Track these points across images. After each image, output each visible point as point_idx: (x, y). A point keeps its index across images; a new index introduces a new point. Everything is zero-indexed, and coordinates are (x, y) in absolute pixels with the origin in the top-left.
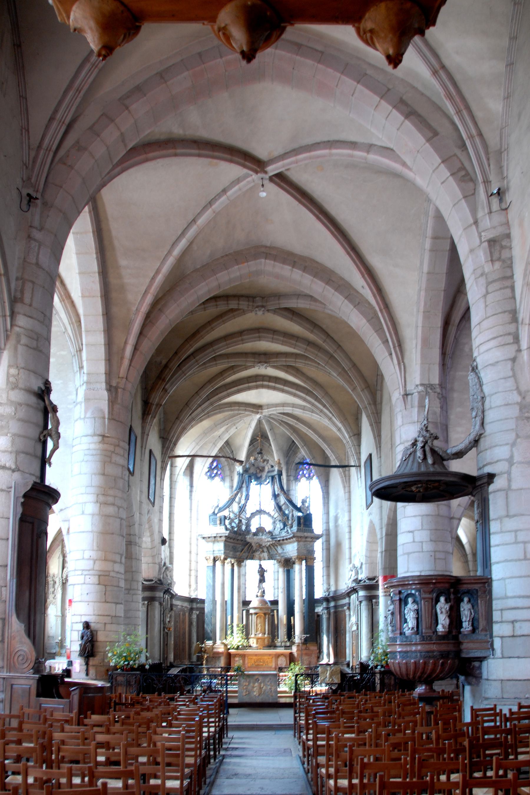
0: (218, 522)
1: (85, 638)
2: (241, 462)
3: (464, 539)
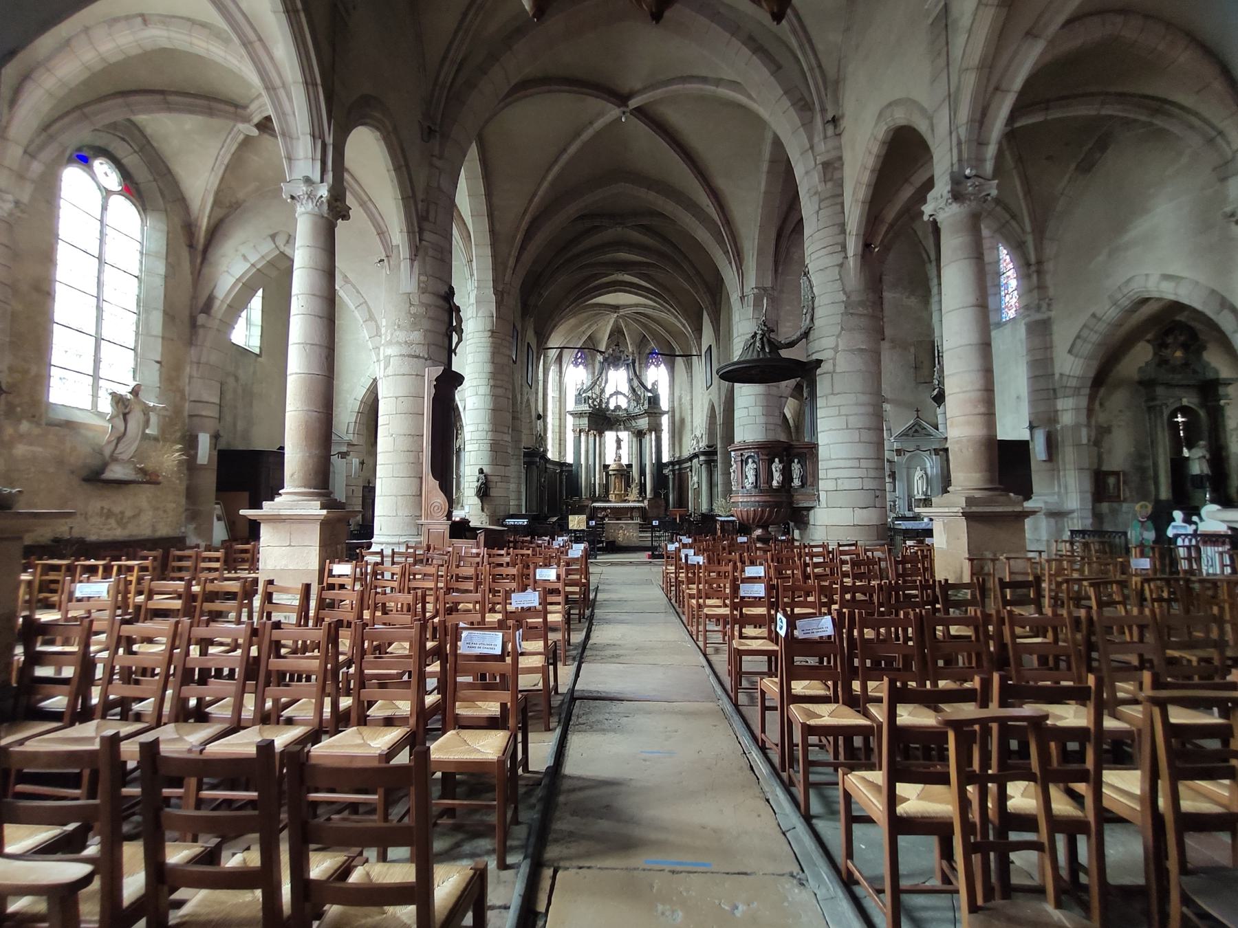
3: (789, 416)
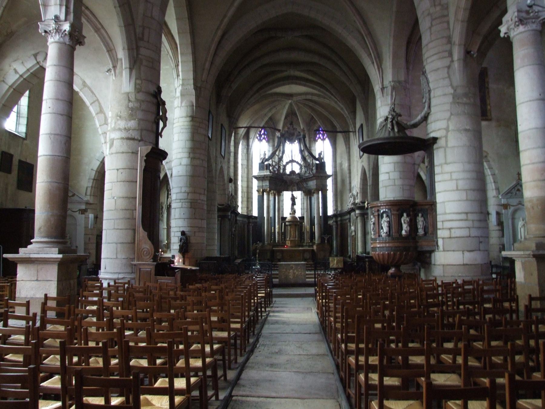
0: (265, 168)
1: (182, 241)
2: (279, 131)
